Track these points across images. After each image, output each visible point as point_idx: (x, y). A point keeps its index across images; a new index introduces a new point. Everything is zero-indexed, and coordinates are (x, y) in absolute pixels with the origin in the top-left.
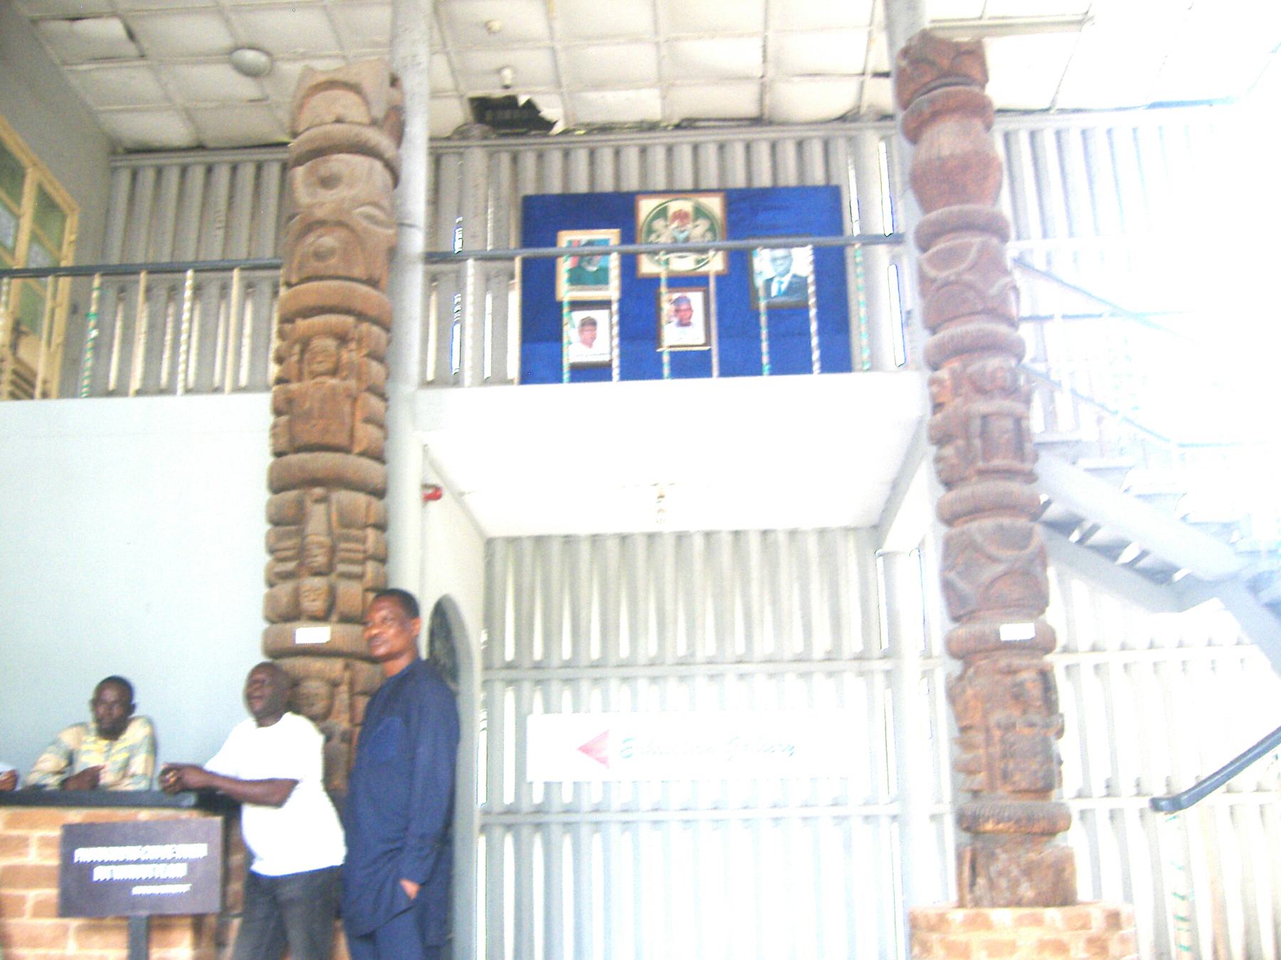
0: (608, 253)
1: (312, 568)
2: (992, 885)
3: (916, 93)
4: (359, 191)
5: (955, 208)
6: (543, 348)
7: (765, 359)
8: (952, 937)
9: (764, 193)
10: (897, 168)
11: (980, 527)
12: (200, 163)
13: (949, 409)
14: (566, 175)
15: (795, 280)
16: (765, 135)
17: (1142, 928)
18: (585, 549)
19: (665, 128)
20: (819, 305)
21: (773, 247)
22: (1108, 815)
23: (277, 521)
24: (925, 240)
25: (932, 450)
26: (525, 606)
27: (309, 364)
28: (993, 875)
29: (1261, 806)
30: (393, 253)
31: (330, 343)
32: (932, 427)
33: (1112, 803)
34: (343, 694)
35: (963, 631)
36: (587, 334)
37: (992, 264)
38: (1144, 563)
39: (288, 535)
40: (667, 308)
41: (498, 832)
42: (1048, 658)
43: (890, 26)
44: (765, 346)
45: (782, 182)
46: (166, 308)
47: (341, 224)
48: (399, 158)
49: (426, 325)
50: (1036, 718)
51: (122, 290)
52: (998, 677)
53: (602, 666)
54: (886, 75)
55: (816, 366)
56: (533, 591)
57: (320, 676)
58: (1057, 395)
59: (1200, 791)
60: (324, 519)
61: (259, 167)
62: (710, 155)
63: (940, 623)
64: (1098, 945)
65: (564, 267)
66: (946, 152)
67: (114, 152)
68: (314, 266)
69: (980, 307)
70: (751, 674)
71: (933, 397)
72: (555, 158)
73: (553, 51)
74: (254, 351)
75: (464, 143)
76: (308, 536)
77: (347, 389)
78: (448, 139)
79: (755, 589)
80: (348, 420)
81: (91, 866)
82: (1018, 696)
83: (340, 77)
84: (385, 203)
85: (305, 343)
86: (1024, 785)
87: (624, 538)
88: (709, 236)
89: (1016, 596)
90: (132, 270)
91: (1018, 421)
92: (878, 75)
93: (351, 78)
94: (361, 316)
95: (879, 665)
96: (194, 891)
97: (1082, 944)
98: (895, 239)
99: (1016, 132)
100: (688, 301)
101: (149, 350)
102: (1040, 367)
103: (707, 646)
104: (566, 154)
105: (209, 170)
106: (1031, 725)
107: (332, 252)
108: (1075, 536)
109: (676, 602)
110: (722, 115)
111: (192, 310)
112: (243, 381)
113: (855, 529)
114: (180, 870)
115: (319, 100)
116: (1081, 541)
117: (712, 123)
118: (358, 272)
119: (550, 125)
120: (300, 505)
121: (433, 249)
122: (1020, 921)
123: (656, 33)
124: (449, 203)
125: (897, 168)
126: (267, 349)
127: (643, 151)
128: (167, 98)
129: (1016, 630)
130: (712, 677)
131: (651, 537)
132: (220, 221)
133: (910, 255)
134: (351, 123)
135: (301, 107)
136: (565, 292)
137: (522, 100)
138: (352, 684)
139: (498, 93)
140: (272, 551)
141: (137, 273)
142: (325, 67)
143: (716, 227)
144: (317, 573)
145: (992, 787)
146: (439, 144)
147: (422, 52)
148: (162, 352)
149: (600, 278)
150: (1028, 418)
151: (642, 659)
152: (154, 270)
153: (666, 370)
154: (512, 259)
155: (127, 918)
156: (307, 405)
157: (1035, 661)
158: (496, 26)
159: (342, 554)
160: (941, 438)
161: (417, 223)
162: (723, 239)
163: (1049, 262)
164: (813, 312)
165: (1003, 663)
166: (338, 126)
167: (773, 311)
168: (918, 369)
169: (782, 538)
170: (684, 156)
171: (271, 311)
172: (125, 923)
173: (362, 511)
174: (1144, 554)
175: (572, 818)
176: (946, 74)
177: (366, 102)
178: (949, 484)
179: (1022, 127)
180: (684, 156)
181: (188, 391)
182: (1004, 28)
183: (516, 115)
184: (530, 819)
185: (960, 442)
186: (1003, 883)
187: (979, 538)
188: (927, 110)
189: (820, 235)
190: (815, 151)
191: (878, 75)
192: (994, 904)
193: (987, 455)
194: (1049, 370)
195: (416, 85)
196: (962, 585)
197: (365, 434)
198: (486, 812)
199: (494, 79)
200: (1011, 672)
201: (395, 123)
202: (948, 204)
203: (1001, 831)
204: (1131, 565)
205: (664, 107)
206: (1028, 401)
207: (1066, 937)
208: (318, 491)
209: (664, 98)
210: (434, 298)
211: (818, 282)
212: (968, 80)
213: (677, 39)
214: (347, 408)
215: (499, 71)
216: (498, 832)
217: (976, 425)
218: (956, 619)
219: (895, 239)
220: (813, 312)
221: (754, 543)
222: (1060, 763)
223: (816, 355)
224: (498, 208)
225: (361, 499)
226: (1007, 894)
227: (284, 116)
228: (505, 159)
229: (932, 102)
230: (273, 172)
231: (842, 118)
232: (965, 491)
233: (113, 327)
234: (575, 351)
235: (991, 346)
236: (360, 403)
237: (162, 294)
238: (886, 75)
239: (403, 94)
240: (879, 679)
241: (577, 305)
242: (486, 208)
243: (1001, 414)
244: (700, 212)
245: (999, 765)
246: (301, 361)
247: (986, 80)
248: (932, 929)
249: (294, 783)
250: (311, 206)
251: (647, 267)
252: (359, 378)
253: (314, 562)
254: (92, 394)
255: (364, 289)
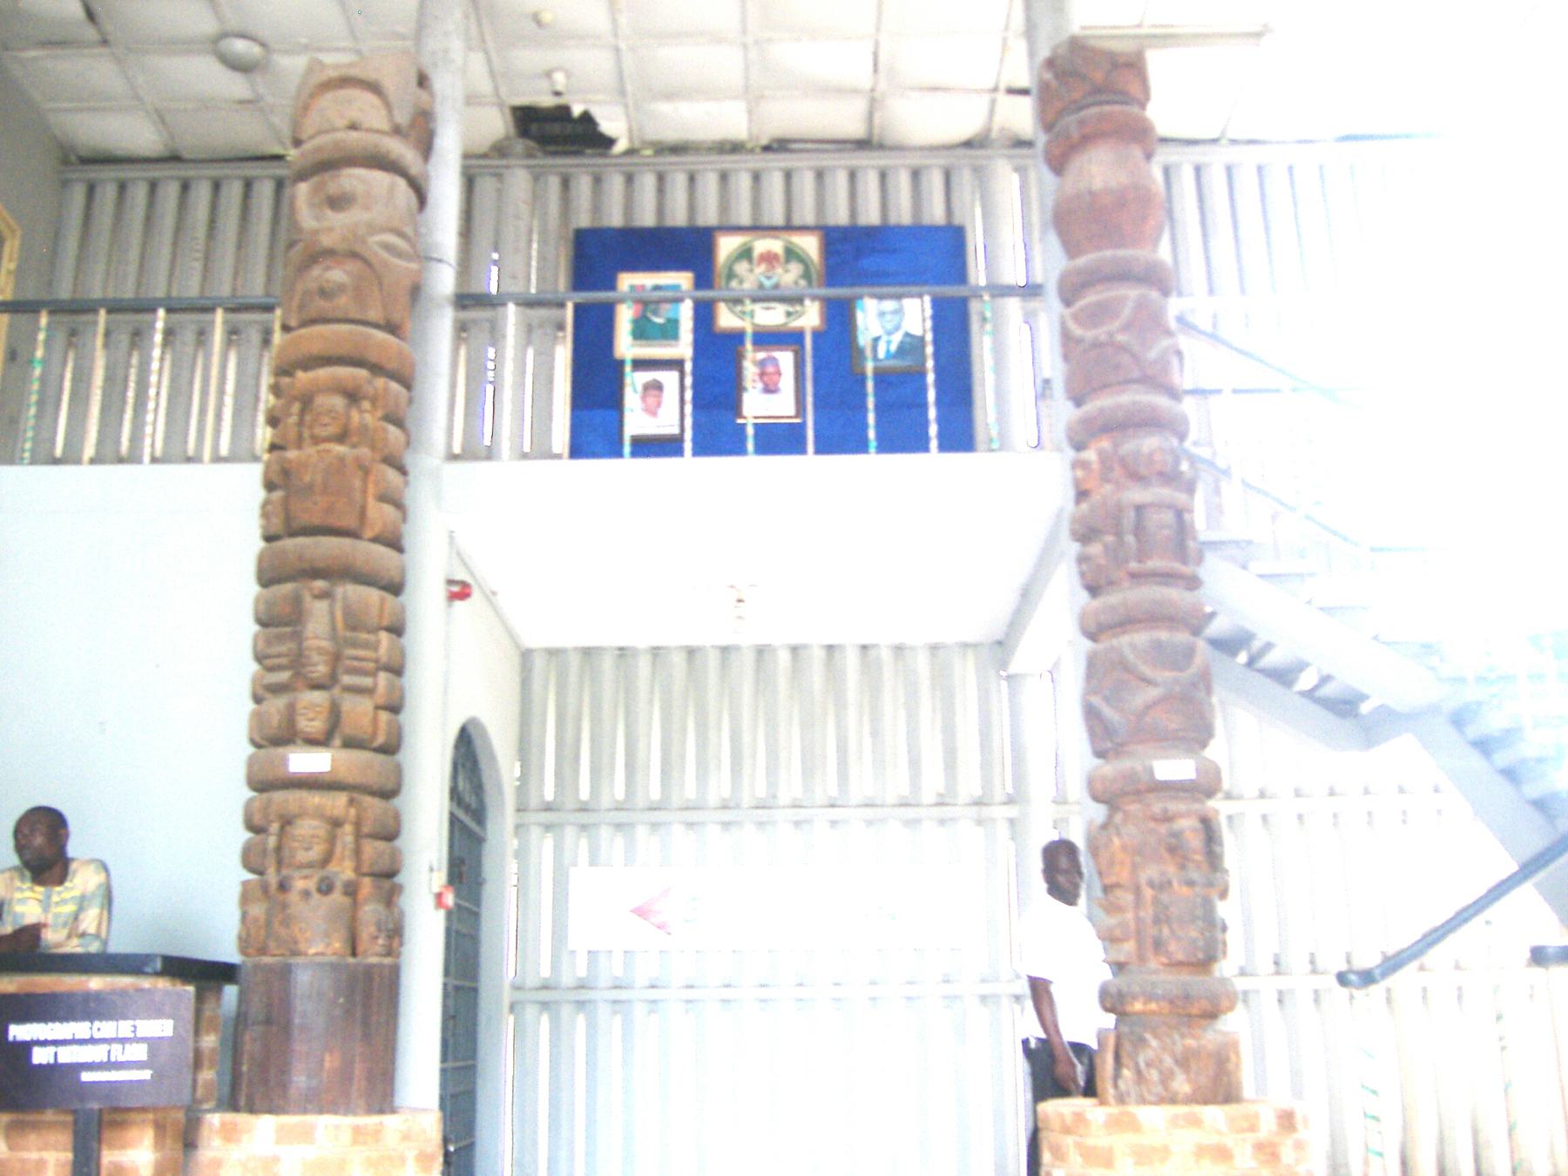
0: (679, 300)
1: (311, 679)
2: (1140, 1076)
3: (1060, 114)
4: (378, 214)
5: (1108, 253)
6: (599, 416)
7: (872, 434)
8: (1090, 1141)
9: (870, 232)
10: (1035, 205)
11: (1133, 642)
12: (172, 178)
13: (1096, 498)
14: (629, 206)
15: (908, 340)
16: (873, 162)
17: (1315, 1134)
18: (644, 666)
19: (752, 151)
20: (938, 370)
21: (881, 297)
22: (1275, 997)
23: (265, 621)
24: (1070, 290)
25: (1074, 548)
26: (569, 737)
27: (311, 427)
28: (1142, 1065)
29: (1316, 992)
30: (416, 291)
31: (338, 402)
32: (1075, 520)
33: (1282, 982)
34: (347, 834)
35: (1109, 769)
36: (651, 400)
37: (1150, 322)
38: (1327, 691)
39: (280, 638)
40: (750, 370)
41: (530, 1012)
42: (1212, 804)
43: (1030, 31)
44: (871, 418)
45: (893, 220)
46: (130, 355)
47: (354, 255)
48: (426, 177)
49: (453, 386)
50: (1195, 875)
51: (73, 333)
52: (1152, 825)
53: (665, 809)
54: (1024, 92)
55: (934, 444)
56: (579, 719)
57: (319, 814)
58: (1224, 485)
59: (1393, 964)
60: (326, 619)
61: (248, 185)
62: (806, 185)
63: (1079, 758)
64: (1268, 1152)
65: (625, 317)
66: (1098, 184)
67: (65, 162)
68: (320, 305)
69: (1136, 374)
70: (808, 821)
71: (1077, 483)
72: (616, 184)
73: (617, 50)
74: (237, 413)
75: (504, 162)
76: (307, 639)
77: (357, 460)
78: (485, 156)
79: (852, 715)
80: (358, 496)
81: (27, 1047)
82: (1175, 848)
83: (353, 72)
84: (409, 230)
85: (307, 401)
86: (1180, 956)
87: (691, 652)
88: (803, 283)
89: (1173, 726)
90: (89, 308)
91: (1180, 513)
92: (1012, 91)
93: (369, 74)
94: (376, 369)
95: (1001, 813)
96: (159, 1076)
97: (1248, 1149)
98: (1031, 291)
99: (1178, 166)
100: (776, 365)
101: (105, 409)
102: (1204, 452)
103: (791, 786)
104: (630, 179)
105: (185, 187)
106: (1191, 883)
107: (341, 288)
108: (1242, 658)
109: (755, 727)
110: (819, 135)
111: (162, 359)
112: (224, 450)
113: (975, 646)
114: (139, 1052)
115: (328, 100)
116: (1251, 663)
117: (809, 146)
118: (374, 314)
119: (609, 142)
120: (297, 601)
121: (466, 290)
122: (1174, 1121)
123: (744, 31)
124: (483, 234)
125: (1035, 205)
126: (255, 408)
127: (724, 177)
128: (137, 97)
129: (1173, 768)
130: (797, 824)
131: (725, 650)
132: (197, 251)
133: (1050, 312)
134: (368, 130)
135: (306, 108)
136: (625, 346)
137: (577, 110)
138: (358, 824)
139: (547, 101)
140: (259, 658)
141: (95, 311)
142: (335, 61)
143: (813, 270)
144: (316, 686)
145: (1142, 959)
146: (474, 162)
147: (456, 45)
148: (122, 411)
149: (669, 332)
150: (1191, 511)
151: (713, 799)
152: (115, 308)
153: (750, 446)
154: (562, 305)
155: (74, 1112)
156: (307, 478)
157: (1196, 806)
158: (547, 17)
159: (348, 662)
160: (1085, 533)
161: (445, 258)
162: (820, 286)
163: (1215, 325)
164: (931, 378)
165: (1157, 808)
166: (354, 135)
167: (882, 377)
168: (1059, 449)
169: (886, 655)
170: (774, 186)
171: (260, 363)
172: (70, 1118)
173: (374, 611)
174: (1325, 680)
175: (585, 995)
176: (1097, 90)
177: (388, 105)
178: (1093, 590)
179: (1185, 160)
180: (774, 186)
181: (154, 460)
182: (1166, 39)
183: (569, 129)
184: (573, 996)
185: (1110, 539)
186: (1154, 1075)
187: (1131, 657)
188: (1076, 135)
189: (938, 284)
190: (934, 183)
191: (1012, 91)
192: (1143, 1101)
193: (1142, 556)
194: (1214, 454)
195: (447, 85)
196: (1107, 712)
197: (379, 514)
198: (517, 988)
199: (544, 84)
200: (1167, 818)
201: (422, 133)
202: (1098, 248)
203: (1154, 1013)
204: (1309, 694)
205: (750, 129)
206: (1190, 489)
207: (1229, 1140)
208: (320, 584)
209: (750, 112)
210: (463, 352)
211: (936, 342)
212: (1125, 98)
213: (770, 40)
214: (357, 483)
215: (548, 74)
216: (530, 1012)
217: (1129, 518)
218: (1100, 754)
219: (1031, 291)
220: (931, 378)
221: (852, 660)
222: (1224, 929)
223: (933, 430)
224: (543, 242)
225: (373, 595)
226: (1159, 1089)
227: (282, 123)
228: (554, 182)
229: (1082, 123)
230: (265, 191)
231: (968, 144)
232: (1112, 599)
233: (62, 377)
234: (636, 421)
235: (1150, 421)
236: (372, 478)
237: (124, 339)
238: (1024, 92)
239: (432, 95)
240: (1003, 829)
241: (640, 364)
242: (530, 241)
243: (1160, 506)
244: (791, 254)
245: (1152, 931)
246: (301, 423)
247: (1147, 98)
248: (1067, 1130)
249: (632, 911)
250: (316, 232)
251: (726, 319)
252: (373, 447)
253: (313, 672)
254: (33, 462)
255: (380, 335)
